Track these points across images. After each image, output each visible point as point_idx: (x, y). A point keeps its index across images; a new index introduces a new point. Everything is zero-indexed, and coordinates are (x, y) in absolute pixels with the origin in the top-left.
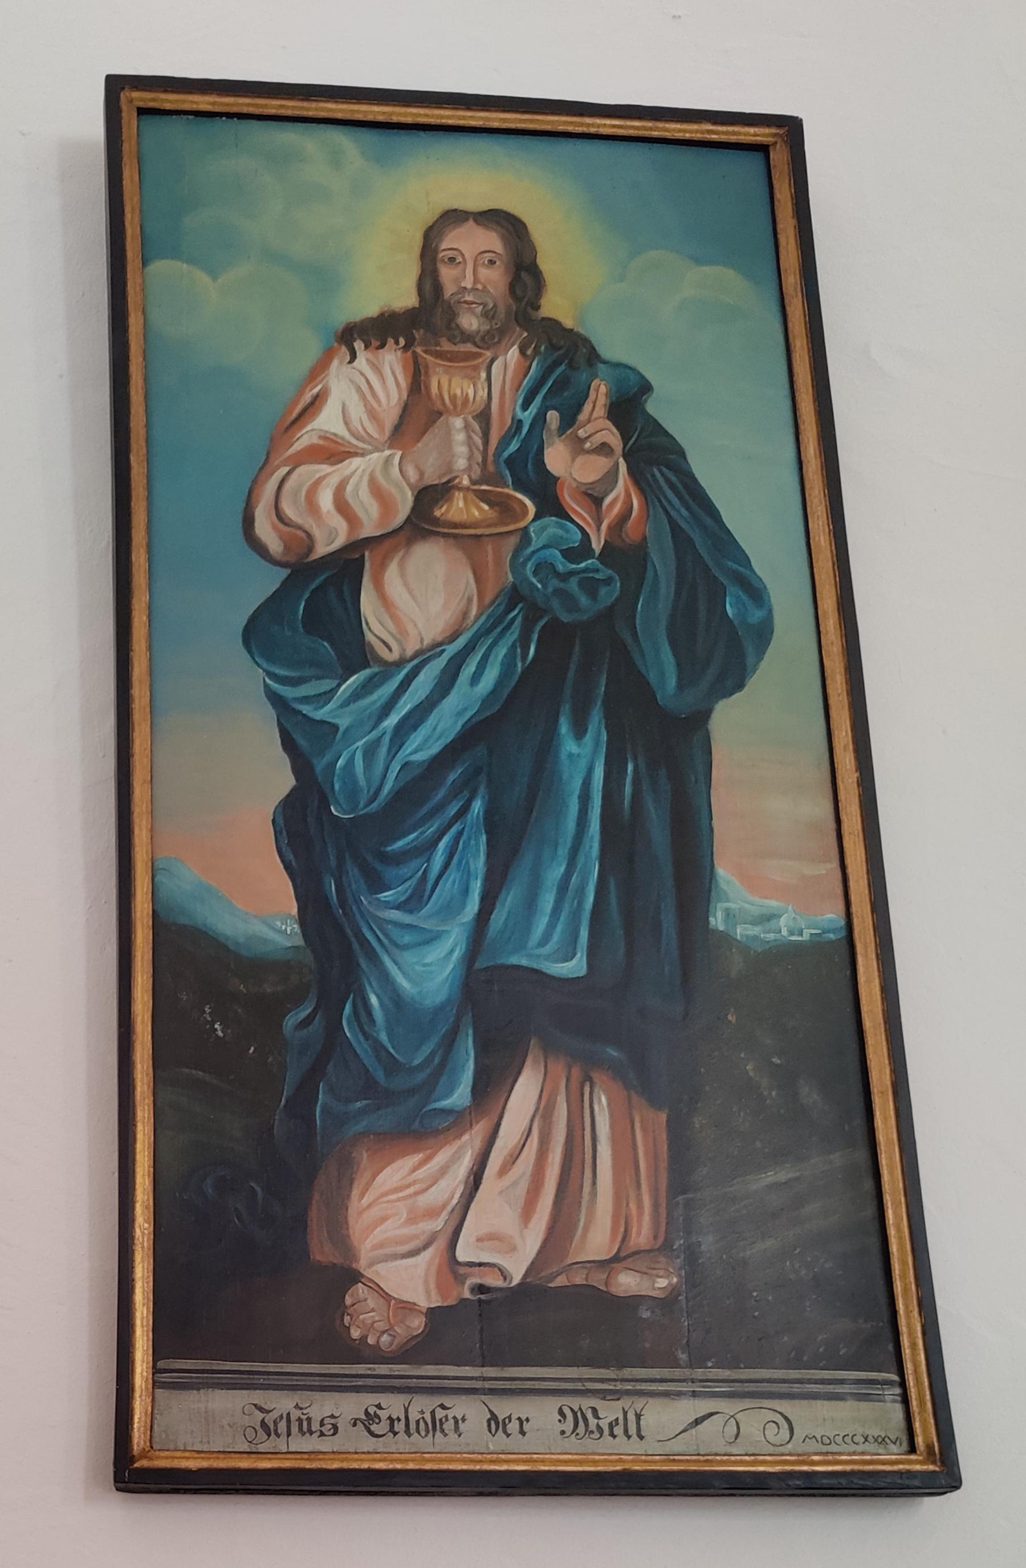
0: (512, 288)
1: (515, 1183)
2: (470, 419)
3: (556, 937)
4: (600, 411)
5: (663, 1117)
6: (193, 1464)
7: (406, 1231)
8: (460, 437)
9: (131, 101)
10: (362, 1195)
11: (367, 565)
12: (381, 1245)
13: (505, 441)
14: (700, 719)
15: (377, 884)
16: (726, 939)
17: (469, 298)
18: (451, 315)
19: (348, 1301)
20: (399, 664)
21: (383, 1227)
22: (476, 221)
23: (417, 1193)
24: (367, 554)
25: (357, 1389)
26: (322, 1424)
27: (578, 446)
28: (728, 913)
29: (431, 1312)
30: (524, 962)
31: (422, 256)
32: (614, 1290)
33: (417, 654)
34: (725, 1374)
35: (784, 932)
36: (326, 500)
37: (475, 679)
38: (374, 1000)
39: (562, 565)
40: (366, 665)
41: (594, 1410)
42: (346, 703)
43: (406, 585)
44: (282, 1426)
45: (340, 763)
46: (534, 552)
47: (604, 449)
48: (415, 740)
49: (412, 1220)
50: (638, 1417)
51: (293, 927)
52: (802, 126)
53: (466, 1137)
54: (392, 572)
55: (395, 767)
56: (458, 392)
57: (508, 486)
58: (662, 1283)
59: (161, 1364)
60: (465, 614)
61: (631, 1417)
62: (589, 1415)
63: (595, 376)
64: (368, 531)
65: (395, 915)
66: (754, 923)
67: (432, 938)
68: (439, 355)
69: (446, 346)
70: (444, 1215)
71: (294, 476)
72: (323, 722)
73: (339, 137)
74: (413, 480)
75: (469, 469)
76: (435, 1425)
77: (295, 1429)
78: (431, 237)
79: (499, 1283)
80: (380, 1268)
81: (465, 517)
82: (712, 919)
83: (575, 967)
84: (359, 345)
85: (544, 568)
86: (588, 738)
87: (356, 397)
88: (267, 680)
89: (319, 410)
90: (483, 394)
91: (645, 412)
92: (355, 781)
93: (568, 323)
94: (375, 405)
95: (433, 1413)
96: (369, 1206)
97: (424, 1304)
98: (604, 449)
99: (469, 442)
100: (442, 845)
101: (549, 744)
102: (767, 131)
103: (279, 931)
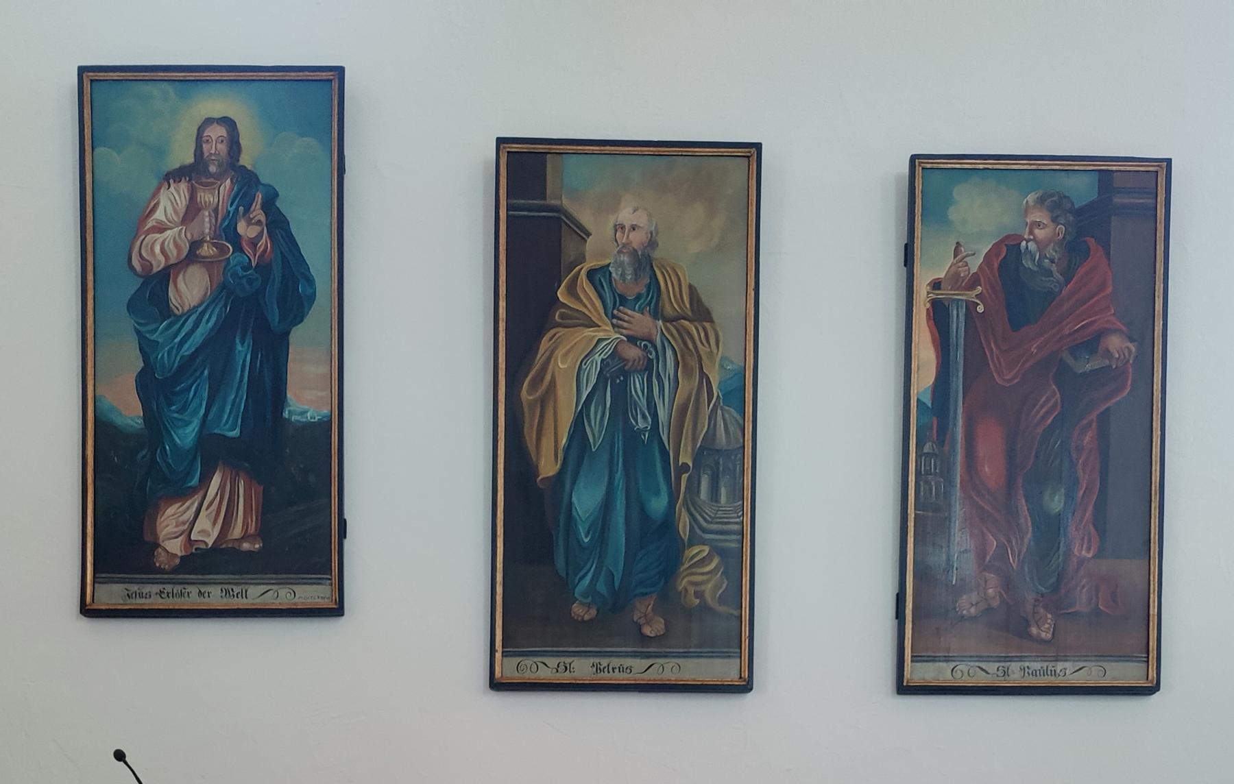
0: (229, 153)
1: (211, 513)
2: (211, 212)
3: (230, 422)
4: (259, 206)
5: (262, 487)
6: (103, 607)
7: (176, 529)
8: (207, 219)
9: (88, 77)
10: (161, 518)
11: (172, 275)
12: (167, 534)
13: (223, 220)
14: (287, 334)
15: (171, 404)
16: (289, 420)
17: (213, 158)
18: (207, 166)
19: (156, 554)
20: (181, 316)
21: (168, 528)
22: (218, 123)
23: (179, 517)
24: (172, 272)
25: (157, 583)
26: (146, 594)
27: (249, 223)
28: (289, 411)
29: (182, 557)
30: (219, 432)
31: (197, 139)
32: (241, 549)
33: (188, 312)
34: (274, 576)
35: (309, 418)
36: (157, 249)
37: (208, 321)
38: (167, 447)
39: (241, 273)
40: (169, 317)
41: (232, 590)
42: (162, 333)
43: (185, 283)
44: (134, 595)
45: (159, 357)
46: (231, 268)
47: (259, 223)
48: (186, 346)
49: (177, 526)
50: (246, 592)
51: (140, 421)
52: (344, 71)
53: (196, 497)
54: (181, 277)
55: (178, 358)
56: (207, 200)
57: (222, 240)
58: (257, 546)
59: (504, 650)
60: (206, 293)
61: (244, 591)
62: (230, 590)
63: (258, 190)
64: (172, 261)
65: (176, 415)
66: (299, 415)
67: (188, 424)
68: (201, 184)
69: (204, 180)
70: (188, 524)
71: (147, 238)
72: (154, 341)
73: (165, 86)
74: (189, 239)
75: (209, 233)
76: (182, 594)
77: (138, 596)
78: (201, 130)
79: (204, 547)
80: (166, 542)
81: (207, 254)
82: (284, 414)
83: (235, 433)
84: (171, 181)
85: (235, 274)
86: (246, 344)
87: (169, 204)
88: (136, 325)
89: (155, 211)
90: (216, 200)
91: (275, 205)
92: (164, 363)
93: (249, 167)
94: (176, 206)
95: (181, 591)
96: (164, 521)
97: (180, 554)
98: (259, 223)
99: (210, 221)
100: (193, 388)
101: (232, 349)
102: (330, 74)
103: (136, 423)
